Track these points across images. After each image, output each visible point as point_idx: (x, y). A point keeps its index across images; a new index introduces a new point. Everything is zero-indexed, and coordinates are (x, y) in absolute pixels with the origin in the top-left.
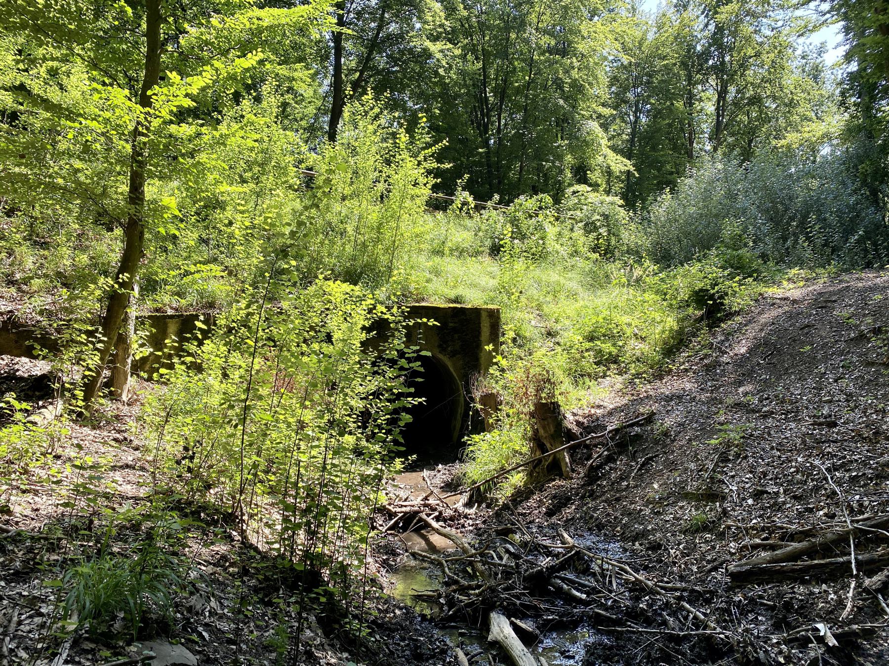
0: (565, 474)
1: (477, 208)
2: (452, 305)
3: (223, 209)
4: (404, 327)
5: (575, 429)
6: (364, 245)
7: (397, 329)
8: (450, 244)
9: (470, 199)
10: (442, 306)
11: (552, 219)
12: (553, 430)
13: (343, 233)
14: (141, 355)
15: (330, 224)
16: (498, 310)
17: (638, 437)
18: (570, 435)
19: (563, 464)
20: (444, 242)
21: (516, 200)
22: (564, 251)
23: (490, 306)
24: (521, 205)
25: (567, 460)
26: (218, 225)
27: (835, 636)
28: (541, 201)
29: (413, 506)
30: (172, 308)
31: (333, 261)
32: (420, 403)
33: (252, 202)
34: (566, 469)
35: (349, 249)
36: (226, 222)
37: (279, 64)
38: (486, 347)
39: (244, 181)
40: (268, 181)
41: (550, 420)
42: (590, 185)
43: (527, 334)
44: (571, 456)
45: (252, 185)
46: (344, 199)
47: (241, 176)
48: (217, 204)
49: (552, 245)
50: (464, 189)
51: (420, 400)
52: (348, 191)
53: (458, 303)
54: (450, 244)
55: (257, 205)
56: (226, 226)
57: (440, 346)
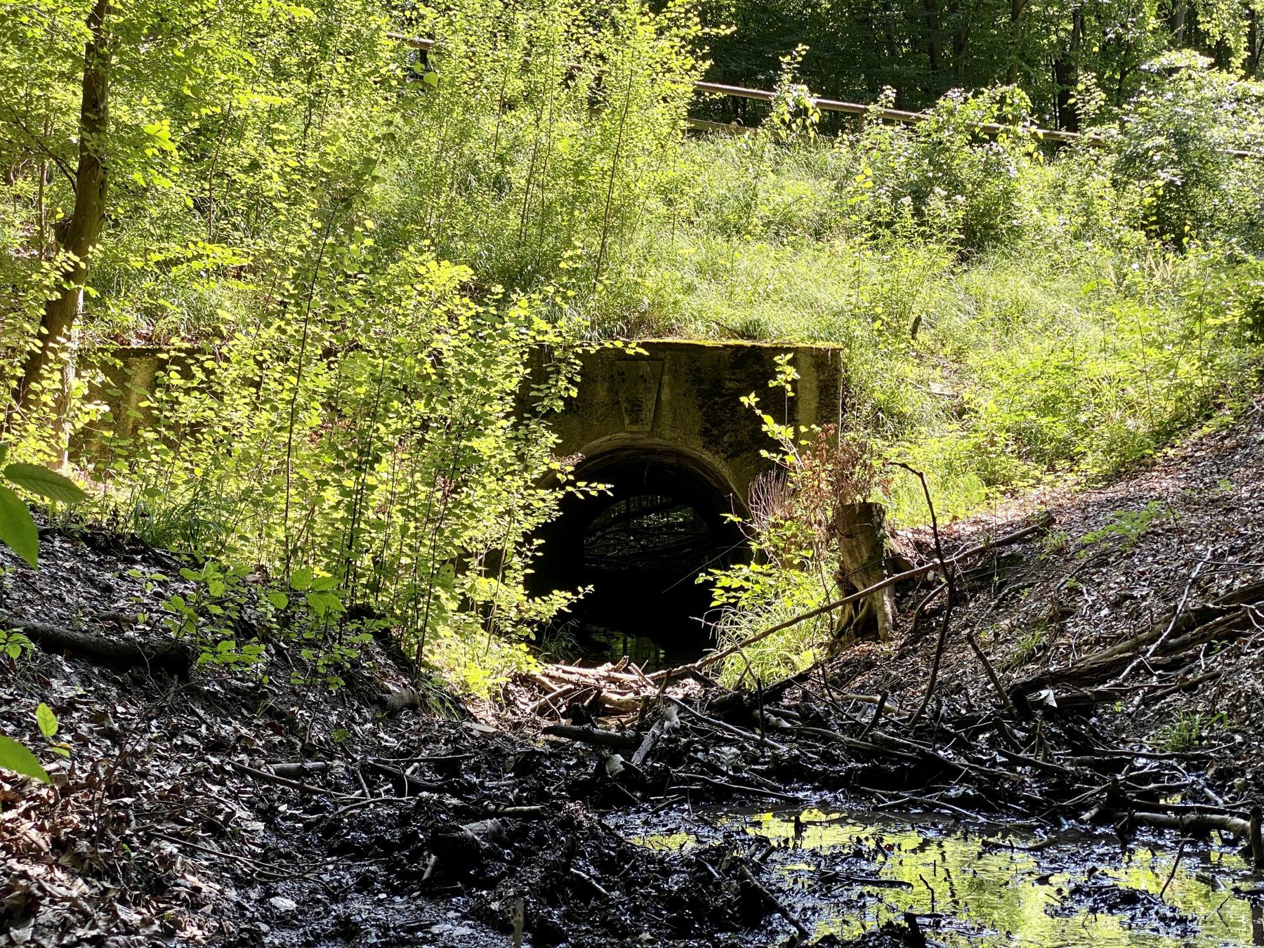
0: (881, 633)
1: (831, 126)
2: (732, 342)
3: (239, 135)
4: (577, 356)
5: (909, 553)
6: (547, 211)
7: (564, 360)
8: (764, 210)
9: (810, 101)
10: (710, 343)
11: (1031, 147)
12: (866, 556)
13: (499, 185)
14: (87, 419)
15: (472, 166)
16: (835, 353)
17: (1014, 559)
18: (897, 563)
19: (880, 617)
20: (748, 205)
21: (941, 102)
22: (1054, 223)
23: (820, 344)
24: (951, 113)
25: (888, 609)
26: (229, 170)
27: (1057, 700)
28: (1002, 101)
29: (585, 676)
30: (139, 336)
31: (476, 248)
32: (601, 493)
33: (299, 120)
34: (884, 625)
35: (514, 221)
36: (246, 162)
37: (210, 242)
38: (743, 399)
39: (280, 73)
40: (334, 71)
41: (861, 538)
42: (1207, 51)
43: (908, 410)
44: (898, 603)
45: (299, 86)
46: (508, 105)
47: (275, 64)
48: (229, 126)
49: (1028, 210)
50: (795, 80)
51: (601, 487)
52: (516, 85)
53: (750, 337)
54: (764, 210)
55: (307, 126)
56: (245, 171)
57: (705, 432)
